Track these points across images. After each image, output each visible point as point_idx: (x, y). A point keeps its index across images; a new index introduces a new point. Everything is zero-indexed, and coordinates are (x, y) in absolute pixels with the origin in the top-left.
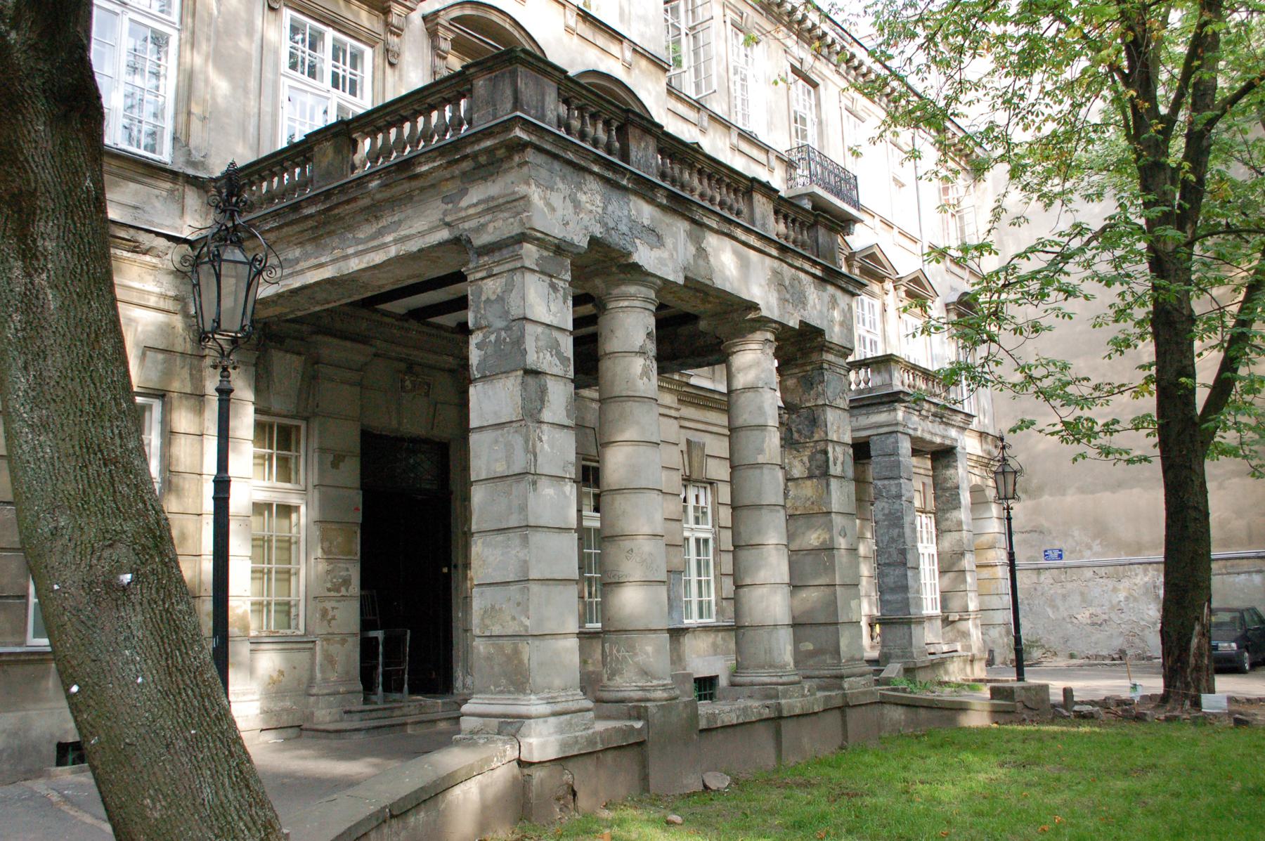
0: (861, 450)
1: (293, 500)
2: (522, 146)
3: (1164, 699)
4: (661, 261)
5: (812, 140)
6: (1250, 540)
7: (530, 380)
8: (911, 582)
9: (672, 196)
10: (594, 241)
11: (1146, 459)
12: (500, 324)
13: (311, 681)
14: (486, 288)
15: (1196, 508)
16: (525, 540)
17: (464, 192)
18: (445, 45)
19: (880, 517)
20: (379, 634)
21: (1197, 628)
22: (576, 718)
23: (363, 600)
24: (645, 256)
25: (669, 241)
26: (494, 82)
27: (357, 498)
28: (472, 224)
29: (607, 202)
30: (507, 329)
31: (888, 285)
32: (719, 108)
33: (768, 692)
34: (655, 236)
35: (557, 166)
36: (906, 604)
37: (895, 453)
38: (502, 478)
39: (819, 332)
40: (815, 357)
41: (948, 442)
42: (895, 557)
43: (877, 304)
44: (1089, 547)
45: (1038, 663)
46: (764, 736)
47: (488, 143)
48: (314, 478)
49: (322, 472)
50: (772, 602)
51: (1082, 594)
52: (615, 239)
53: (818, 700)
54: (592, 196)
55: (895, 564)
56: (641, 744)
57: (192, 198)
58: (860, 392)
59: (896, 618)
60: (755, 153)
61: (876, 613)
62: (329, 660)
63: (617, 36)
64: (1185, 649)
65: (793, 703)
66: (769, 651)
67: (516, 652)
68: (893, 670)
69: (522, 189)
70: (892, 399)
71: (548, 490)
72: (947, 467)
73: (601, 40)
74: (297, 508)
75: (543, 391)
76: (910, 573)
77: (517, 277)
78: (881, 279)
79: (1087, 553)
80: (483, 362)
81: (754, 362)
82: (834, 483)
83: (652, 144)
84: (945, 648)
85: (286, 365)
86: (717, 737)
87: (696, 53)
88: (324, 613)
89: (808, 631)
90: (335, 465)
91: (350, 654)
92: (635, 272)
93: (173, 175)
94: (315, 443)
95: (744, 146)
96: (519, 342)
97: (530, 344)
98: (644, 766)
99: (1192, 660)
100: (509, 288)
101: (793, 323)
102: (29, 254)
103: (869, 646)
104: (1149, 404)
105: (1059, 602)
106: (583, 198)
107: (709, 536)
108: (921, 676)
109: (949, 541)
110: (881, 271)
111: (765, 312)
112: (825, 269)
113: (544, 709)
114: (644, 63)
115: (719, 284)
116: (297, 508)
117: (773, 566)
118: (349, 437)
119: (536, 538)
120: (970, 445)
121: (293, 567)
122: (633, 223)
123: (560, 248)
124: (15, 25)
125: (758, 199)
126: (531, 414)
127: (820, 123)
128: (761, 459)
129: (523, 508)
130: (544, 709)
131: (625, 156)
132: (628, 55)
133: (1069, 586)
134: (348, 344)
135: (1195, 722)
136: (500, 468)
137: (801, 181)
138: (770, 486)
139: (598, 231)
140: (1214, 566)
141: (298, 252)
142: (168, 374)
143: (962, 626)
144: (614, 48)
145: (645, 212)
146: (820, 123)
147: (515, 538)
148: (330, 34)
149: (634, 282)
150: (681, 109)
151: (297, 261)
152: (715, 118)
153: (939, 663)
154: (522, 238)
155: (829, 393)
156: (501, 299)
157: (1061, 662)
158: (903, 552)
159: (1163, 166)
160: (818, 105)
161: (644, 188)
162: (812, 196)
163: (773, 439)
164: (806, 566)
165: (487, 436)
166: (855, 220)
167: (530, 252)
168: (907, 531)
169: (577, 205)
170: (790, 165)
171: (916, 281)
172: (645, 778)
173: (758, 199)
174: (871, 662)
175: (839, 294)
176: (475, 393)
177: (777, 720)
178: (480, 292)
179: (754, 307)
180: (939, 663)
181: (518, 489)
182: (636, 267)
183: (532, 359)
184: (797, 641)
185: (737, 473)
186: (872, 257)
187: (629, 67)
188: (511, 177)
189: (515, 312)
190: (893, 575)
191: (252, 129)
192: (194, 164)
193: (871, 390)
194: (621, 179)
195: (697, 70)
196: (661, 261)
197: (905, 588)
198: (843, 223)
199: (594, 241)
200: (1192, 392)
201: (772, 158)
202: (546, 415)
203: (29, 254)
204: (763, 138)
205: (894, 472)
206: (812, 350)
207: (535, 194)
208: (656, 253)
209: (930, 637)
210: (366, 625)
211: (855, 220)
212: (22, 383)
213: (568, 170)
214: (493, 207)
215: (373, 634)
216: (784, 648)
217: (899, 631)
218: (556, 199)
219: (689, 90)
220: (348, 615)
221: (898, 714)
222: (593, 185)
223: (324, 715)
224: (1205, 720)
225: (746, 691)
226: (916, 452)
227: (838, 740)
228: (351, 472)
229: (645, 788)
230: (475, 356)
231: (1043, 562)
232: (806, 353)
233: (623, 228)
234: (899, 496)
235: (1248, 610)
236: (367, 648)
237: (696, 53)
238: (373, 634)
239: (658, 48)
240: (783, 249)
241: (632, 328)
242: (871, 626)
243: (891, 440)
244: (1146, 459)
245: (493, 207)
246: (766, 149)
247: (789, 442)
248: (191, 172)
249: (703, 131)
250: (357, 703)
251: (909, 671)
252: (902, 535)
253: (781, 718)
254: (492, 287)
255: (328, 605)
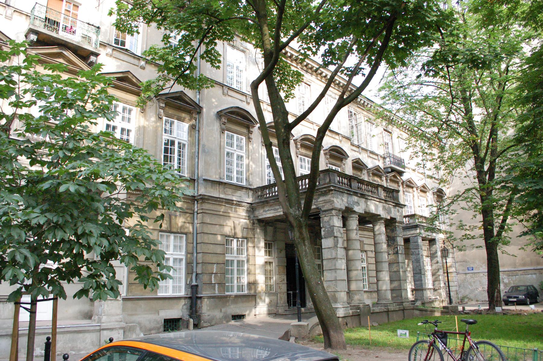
0: (407, 241)
1: (271, 261)
2: (332, 190)
3: (489, 309)
4: (359, 209)
5: (391, 152)
6: (531, 264)
7: (335, 239)
8: (423, 278)
9: (361, 194)
10: (346, 207)
11: (481, 247)
12: (328, 227)
13: (277, 303)
14: (325, 219)
15: (494, 259)
16: (336, 272)
17: (319, 198)
18: (299, 146)
19: (413, 260)
20: (291, 292)
21: (496, 290)
22: (347, 309)
23: (287, 284)
24: (356, 209)
25: (361, 204)
26: (325, 176)
27: (285, 260)
28: (321, 205)
29: (348, 198)
30: (330, 228)
31: (415, 189)
32: (363, 146)
33: (386, 305)
34: (358, 204)
35: (338, 193)
36: (422, 285)
37: (417, 242)
38: (330, 259)
39: (395, 219)
40: (394, 224)
41: (433, 238)
42: (418, 271)
43: (411, 195)
44: (482, 267)
45: (467, 303)
46: (385, 315)
47: (325, 189)
48: (276, 255)
49: (278, 254)
50: (386, 285)
51: (480, 281)
52: (350, 206)
53: (397, 308)
54: (345, 198)
55: (418, 273)
56: (359, 315)
57: (251, 193)
58: (407, 224)
59: (419, 289)
60: (374, 156)
61: (413, 287)
62: (281, 298)
63: (338, 134)
64: (493, 296)
65: (391, 308)
66: (385, 296)
67: (335, 295)
68: (418, 303)
69: (332, 199)
70: (416, 227)
71: (339, 261)
72: (433, 244)
73: (334, 136)
74: (272, 263)
75: (338, 240)
76: (422, 276)
77: (332, 217)
78: (412, 188)
79: (481, 268)
80: (325, 234)
81: (380, 228)
82: (400, 255)
83: (356, 181)
84: (434, 298)
85: (270, 229)
86: (375, 315)
87: (357, 132)
88: (280, 287)
89: (394, 291)
90: (280, 252)
91: (285, 297)
92: (354, 212)
93: (247, 188)
94: (276, 247)
95: (371, 155)
96: (333, 231)
97: (335, 231)
98: (360, 320)
99: (495, 299)
100: (330, 219)
101: (389, 218)
102: (305, 245)
103: (410, 296)
104: (482, 232)
105: (472, 284)
106: (343, 198)
107: (365, 266)
108: (426, 305)
109: (435, 266)
110: (412, 185)
111: (382, 216)
112: (396, 203)
113: (342, 306)
114: (344, 139)
115: (371, 212)
116: (272, 263)
117: (385, 276)
118: (283, 245)
119: (338, 271)
120: (440, 237)
121: (272, 276)
122: (353, 202)
123: (339, 210)
124: (301, 218)
125: (380, 189)
126: (336, 246)
127: (392, 144)
128: (382, 251)
129: (335, 265)
130: (342, 306)
131: (350, 186)
132: (341, 138)
133: (476, 279)
134: (282, 223)
135: (493, 314)
136: (330, 257)
137: (388, 163)
138: (385, 257)
139: (347, 205)
140: (500, 273)
141: (278, 207)
142: (248, 233)
143: (439, 291)
144: (337, 137)
145: (355, 198)
146: (392, 144)
147: (333, 271)
148: (235, 135)
149: (353, 214)
150: (354, 148)
151: (278, 209)
152: (363, 149)
153: (432, 302)
154: (332, 209)
155: (398, 233)
156: (328, 221)
157: (474, 303)
158: (420, 270)
159: (483, 172)
160: (392, 138)
161: (356, 194)
162: (391, 167)
163: (385, 246)
164: (396, 277)
165: (327, 250)
166: (404, 172)
167: (334, 212)
168: (421, 264)
169: (343, 200)
170: (384, 158)
171: (423, 187)
172: (360, 322)
173: (380, 189)
174: (412, 301)
175: (399, 209)
176: (323, 241)
177: (388, 312)
178: (323, 220)
179: (380, 215)
180: (432, 302)
181: (334, 261)
182: (354, 211)
183: (335, 234)
184: (392, 294)
185: (377, 254)
186: (410, 182)
187: (341, 141)
188: (330, 196)
189: (332, 224)
190: (418, 276)
191: (260, 175)
192: (250, 185)
193: (410, 224)
194: (351, 193)
195: (358, 136)
196: (359, 209)
197: (421, 280)
198: (401, 173)
199: (346, 207)
200: (493, 229)
201: (379, 157)
202: (339, 246)
203: (305, 245)
204: (377, 152)
205: (417, 247)
206: (393, 223)
207: (335, 200)
208: (358, 207)
209: (429, 294)
210: (288, 290)
211: (404, 172)
212: (306, 260)
213: (341, 193)
214: (326, 202)
215: (289, 292)
216: (389, 295)
217: (420, 292)
218: (339, 200)
219: (356, 143)
220: (284, 287)
221: (417, 312)
222: (345, 195)
223: (281, 311)
224: (496, 314)
225: (380, 305)
226: (423, 240)
227: (403, 318)
228: (283, 253)
229: (360, 324)
230: (323, 233)
231: (467, 272)
232: (392, 223)
233: (351, 203)
234: (419, 254)
235: (530, 286)
236: (288, 295)
237: (357, 132)
238: (289, 292)
239: (347, 134)
240: (385, 201)
241: (354, 223)
242: (412, 291)
243: (416, 238)
244: (481, 247)
245: (326, 202)
246: (377, 155)
247: (388, 245)
248: (250, 187)
249: (360, 153)
250: (287, 308)
251: (423, 304)
252: (420, 265)
253: (388, 311)
254: (326, 219)
255: (280, 285)
